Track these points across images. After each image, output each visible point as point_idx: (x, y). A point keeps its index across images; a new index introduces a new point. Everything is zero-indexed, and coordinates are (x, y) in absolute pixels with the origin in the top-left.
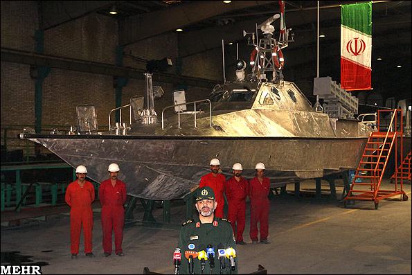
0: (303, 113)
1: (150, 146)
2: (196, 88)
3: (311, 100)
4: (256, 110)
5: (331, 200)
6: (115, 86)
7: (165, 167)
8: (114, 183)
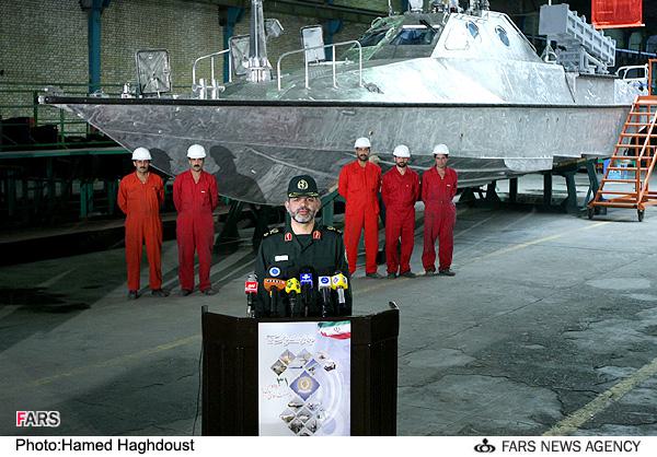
0: (518, 64)
1: (256, 117)
2: (357, 25)
3: (539, 45)
4: (438, 59)
5: (567, 207)
6: (222, 22)
7: (284, 151)
8: (196, 176)
